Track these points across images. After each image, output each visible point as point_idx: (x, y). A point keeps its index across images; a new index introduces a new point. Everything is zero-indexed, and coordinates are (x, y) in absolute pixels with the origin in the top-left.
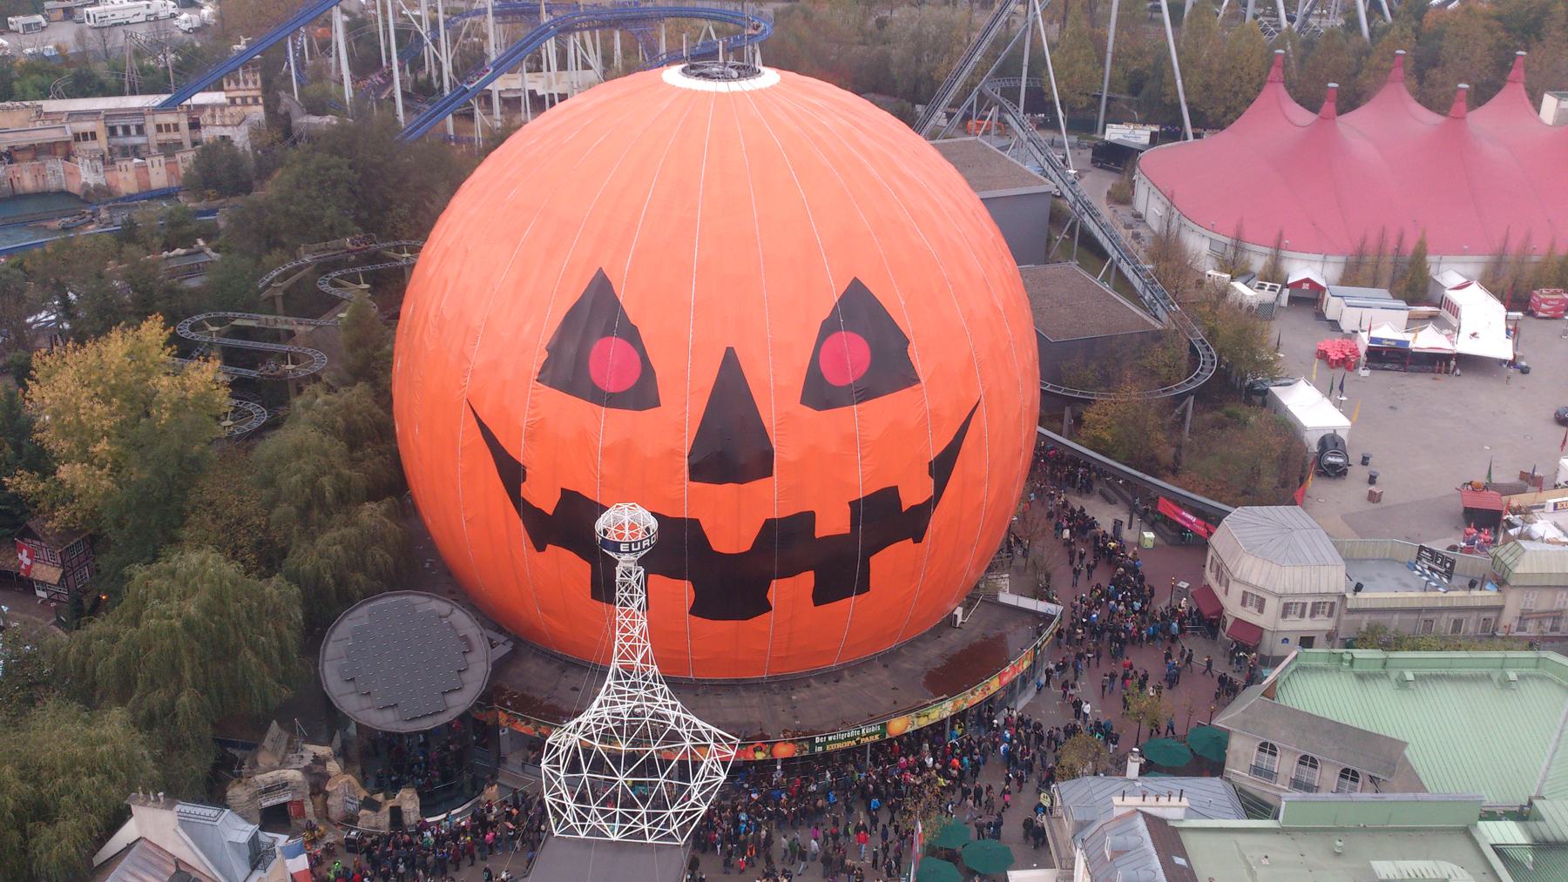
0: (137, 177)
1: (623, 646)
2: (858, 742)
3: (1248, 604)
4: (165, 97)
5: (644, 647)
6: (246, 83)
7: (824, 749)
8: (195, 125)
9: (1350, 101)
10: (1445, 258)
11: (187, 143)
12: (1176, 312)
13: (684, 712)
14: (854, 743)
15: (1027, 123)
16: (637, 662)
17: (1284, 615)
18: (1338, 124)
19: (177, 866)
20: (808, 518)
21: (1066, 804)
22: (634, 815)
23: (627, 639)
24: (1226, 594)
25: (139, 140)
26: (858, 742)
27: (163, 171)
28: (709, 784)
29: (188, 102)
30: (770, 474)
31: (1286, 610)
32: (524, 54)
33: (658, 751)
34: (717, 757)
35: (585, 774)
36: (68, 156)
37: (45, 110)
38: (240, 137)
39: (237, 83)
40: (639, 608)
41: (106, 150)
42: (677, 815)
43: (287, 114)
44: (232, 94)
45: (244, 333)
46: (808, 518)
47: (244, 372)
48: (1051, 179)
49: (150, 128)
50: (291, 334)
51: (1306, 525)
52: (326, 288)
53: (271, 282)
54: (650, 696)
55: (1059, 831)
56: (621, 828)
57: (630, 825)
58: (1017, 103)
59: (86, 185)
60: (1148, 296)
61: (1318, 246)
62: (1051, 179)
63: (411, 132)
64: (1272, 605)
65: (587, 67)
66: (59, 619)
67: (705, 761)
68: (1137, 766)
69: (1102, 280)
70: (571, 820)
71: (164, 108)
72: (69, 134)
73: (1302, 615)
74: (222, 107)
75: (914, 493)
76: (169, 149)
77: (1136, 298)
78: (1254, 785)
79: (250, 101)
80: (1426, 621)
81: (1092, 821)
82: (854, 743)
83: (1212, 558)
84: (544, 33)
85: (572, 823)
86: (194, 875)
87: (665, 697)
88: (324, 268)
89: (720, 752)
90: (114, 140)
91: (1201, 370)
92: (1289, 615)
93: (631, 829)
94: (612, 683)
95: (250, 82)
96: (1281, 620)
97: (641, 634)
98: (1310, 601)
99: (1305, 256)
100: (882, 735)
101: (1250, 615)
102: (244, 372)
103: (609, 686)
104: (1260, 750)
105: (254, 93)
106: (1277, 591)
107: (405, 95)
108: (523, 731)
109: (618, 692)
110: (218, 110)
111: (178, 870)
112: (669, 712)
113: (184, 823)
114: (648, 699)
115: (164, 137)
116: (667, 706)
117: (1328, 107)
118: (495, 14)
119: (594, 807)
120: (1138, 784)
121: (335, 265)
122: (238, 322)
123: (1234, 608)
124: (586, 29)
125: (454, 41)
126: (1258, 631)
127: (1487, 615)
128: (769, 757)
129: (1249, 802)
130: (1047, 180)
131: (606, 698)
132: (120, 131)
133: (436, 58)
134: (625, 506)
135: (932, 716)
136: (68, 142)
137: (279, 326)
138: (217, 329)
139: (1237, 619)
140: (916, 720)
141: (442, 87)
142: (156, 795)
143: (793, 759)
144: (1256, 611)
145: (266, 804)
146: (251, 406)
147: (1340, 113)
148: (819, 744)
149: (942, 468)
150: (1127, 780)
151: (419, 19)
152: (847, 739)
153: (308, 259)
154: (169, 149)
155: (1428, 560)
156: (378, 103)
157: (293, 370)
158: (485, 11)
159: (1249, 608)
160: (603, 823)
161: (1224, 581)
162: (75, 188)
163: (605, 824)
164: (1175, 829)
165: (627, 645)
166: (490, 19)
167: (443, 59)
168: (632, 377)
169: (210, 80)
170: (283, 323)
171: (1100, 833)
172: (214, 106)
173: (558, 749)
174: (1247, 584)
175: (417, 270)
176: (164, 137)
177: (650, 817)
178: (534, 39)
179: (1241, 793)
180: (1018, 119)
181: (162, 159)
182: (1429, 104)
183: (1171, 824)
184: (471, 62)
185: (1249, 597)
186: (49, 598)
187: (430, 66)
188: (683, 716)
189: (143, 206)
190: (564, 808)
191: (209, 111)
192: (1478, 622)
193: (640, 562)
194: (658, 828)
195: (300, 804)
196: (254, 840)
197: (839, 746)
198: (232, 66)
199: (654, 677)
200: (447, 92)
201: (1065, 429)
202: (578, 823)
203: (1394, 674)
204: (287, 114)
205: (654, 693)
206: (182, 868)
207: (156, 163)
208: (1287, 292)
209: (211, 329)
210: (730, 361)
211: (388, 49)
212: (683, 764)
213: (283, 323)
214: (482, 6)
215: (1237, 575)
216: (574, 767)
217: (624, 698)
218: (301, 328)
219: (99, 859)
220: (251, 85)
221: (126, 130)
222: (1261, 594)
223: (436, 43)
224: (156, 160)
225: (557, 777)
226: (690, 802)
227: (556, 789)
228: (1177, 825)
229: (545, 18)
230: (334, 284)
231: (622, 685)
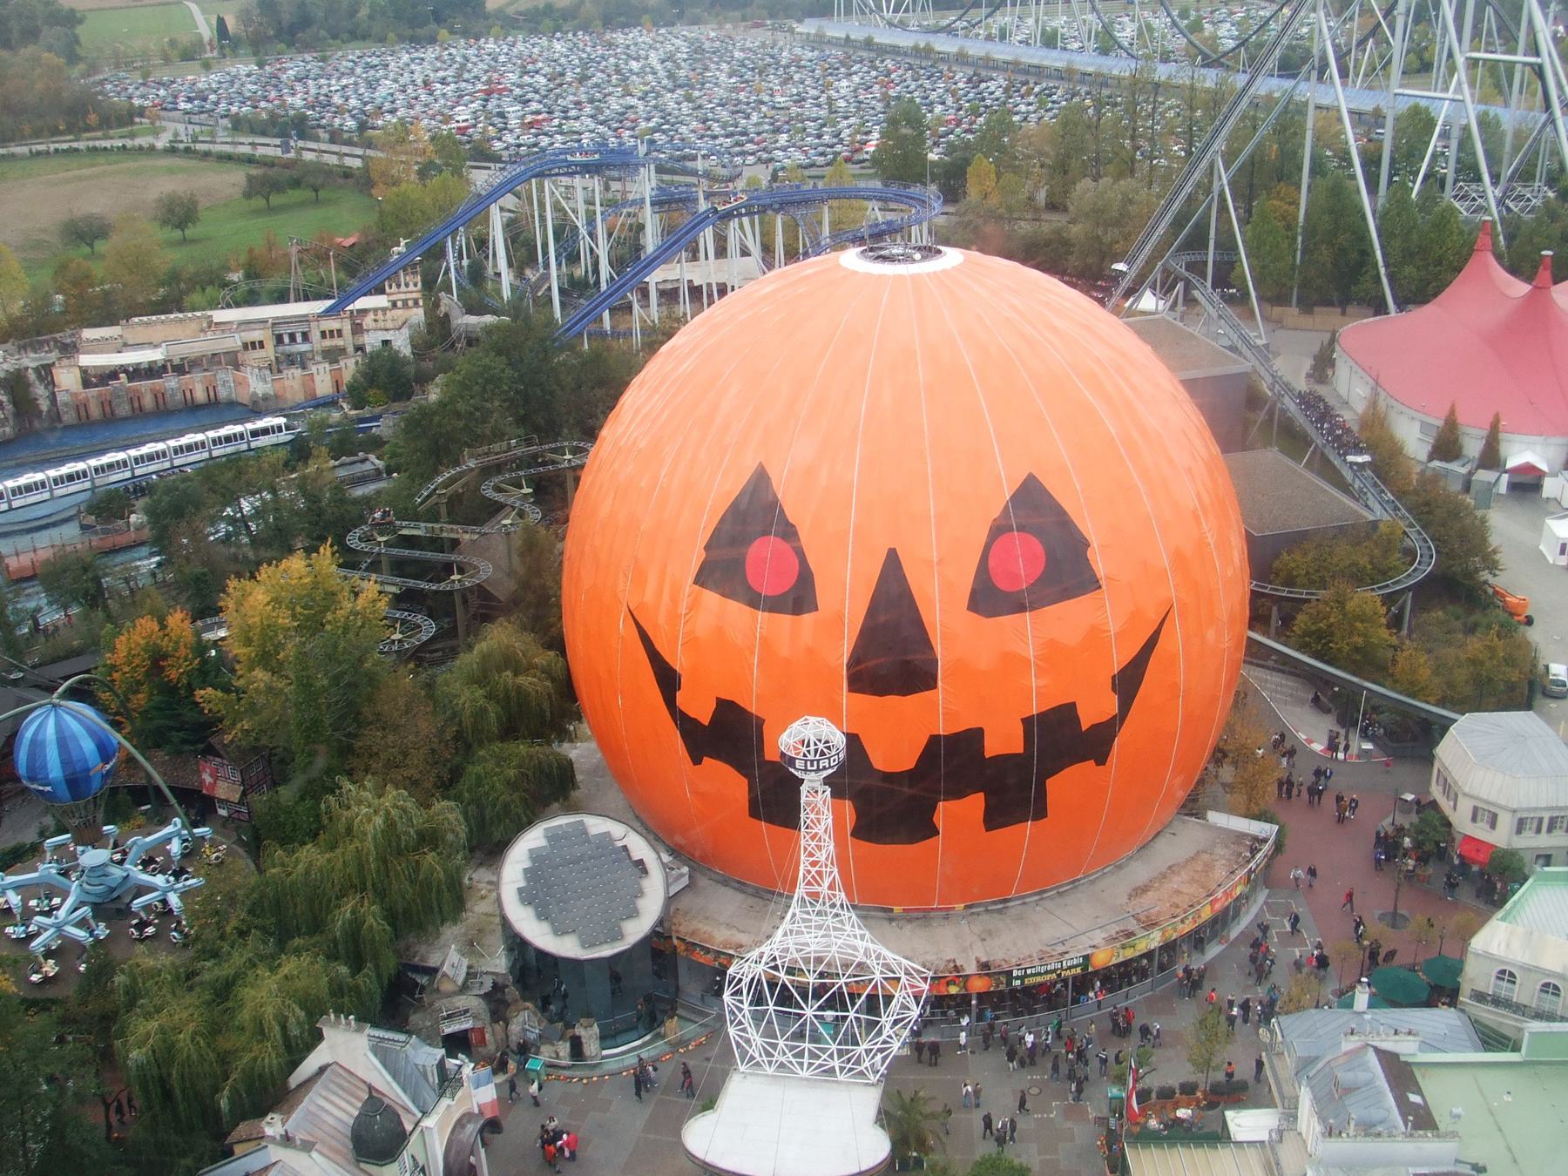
0: (303, 384)
1: (809, 872)
2: (1059, 976)
3: (1479, 818)
4: (329, 303)
5: (831, 873)
6: (407, 285)
7: (1022, 983)
8: (358, 329)
11: (350, 349)
12: (1388, 502)
13: (872, 942)
14: (1054, 976)
15: (1216, 298)
16: (824, 888)
17: (1519, 831)
18: (1555, 296)
19: (370, 1093)
20: (976, 735)
21: (1288, 1040)
22: (823, 1050)
23: (814, 864)
24: (1455, 808)
25: (305, 347)
26: (1059, 976)
27: (328, 378)
28: (903, 1019)
29: (350, 307)
30: (935, 687)
31: (1520, 827)
32: (680, 242)
33: (846, 984)
34: (909, 991)
35: (771, 1007)
36: (237, 366)
37: (216, 320)
38: (402, 343)
39: (399, 286)
40: (826, 831)
41: (273, 358)
42: (868, 1051)
43: (446, 315)
44: (393, 298)
45: (410, 542)
46: (976, 735)
47: (411, 583)
48: (1245, 358)
49: (315, 336)
50: (455, 543)
52: (490, 493)
53: (435, 490)
54: (839, 926)
55: (1281, 1069)
56: (810, 1064)
57: (820, 1061)
59: (255, 394)
60: (1357, 484)
61: (1538, 428)
62: (1245, 358)
63: (569, 329)
64: (1506, 822)
65: (745, 253)
66: (240, 839)
67: (897, 995)
68: (1366, 997)
69: (1306, 466)
70: (756, 1055)
71: (328, 313)
72: (240, 344)
73: (1538, 831)
74: (384, 310)
75: (1096, 707)
76: (332, 355)
77: (1345, 487)
78: (1489, 1015)
79: (410, 303)
81: (1317, 1058)
82: (1054, 976)
84: (700, 222)
85: (759, 1059)
86: (386, 1101)
87: (853, 926)
88: (487, 472)
89: (912, 986)
90: (280, 348)
91: (1420, 563)
93: (821, 1066)
94: (797, 911)
95: (411, 284)
97: (827, 859)
98: (1546, 816)
99: (1524, 438)
100: (1085, 968)
101: (1480, 832)
102: (411, 583)
103: (794, 915)
104: (1498, 978)
105: (415, 295)
106: (1510, 805)
107: (561, 290)
108: (701, 961)
109: (804, 920)
110: (380, 312)
111: (371, 1096)
112: (858, 942)
113: (378, 1049)
114: (835, 929)
115: (328, 343)
116: (855, 936)
117: (1545, 275)
118: (653, 204)
119: (781, 1043)
120: (1366, 1016)
121: (498, 468)
122: (405, 532)
123: (1461, 821)
124: (746, 215)
125: (610, 235)
128: (963, 992)
129: (1483, 1034)
130: (1242, 360)
131: (791, 927)
132: (286, 339)
133: (591, 250)
134: (812, 719)
135: (1138, 948)
136: (236, 353)
137: (444, 535)
138: (385, 539)
140: (1121, 951)
141: (597, 282)
142: (347, 1018)
143: (988, 993)
144: (1487, 827)
145: (448, 1031)
146: (419, 619)
147: (1555, 283)
148: (1017, 978)
149: (1128, 682)
150: (1356, 1013)
151: (575, 211)
152: (1047, 972)
153: (472, 464)
154: (332, 355)
156: (534, 301)
157: (459, 581)
158: (643, 200)
159: (1479, 824)
160: (792, 1059)
162: (244, 398)
163: (794, 1061)
164: (1408, 1064)
165: (813, 870)
168: (790, 580)
169: (372, 285)
170: (448, 531)
171: (1327, 1069)
172: (375, 310)
173: (740, 980)
174: (1477, 798)
175: (587, 479)
176: (328, 343)
177: (841, 1053)
178: (693, 228)
179: (1476, 1023)
180: (1204, 292)
181: (327, 365)
183: (1402, 1059)
184: (629, 256)
186: (230, 816)
188: (871, 946)
189: (310, 413)
190: (748, 1041)
191: (371, 316)
193: (827, 781)
194: (849, 1066)
195: (481, 1031)
196: (441, 1066)
197: (1039, 979)
198: (393, 270)
199: (842, 906)
200: (604, 287)
201: (1273, 630)
202: (765, 1059)
204: (446, 315)
205: (842, 922)
206: (375, 1094)
207: (322, 370)
208: (1505, 477)
209: (380, 539)
210: (893, 560)
211: (545, 245)
212: (872, 998)
213: (448, 531)
214: (638, 196)
215: (1466, 790)
216: (759, 1000)
217: (810, 927)
218: (467, 537)
219: (295, 1079)
220: (411, 288)
221: (292, 337)
222: (1493, 809)
223: (592, 235)
224: (321, 367)
225: (741, 1010)
226: (881, 1039)
227: (740, 1023)
228: (1410, 1060)
229: (703, 206)
230: (499, 490)
231: (808, 913)
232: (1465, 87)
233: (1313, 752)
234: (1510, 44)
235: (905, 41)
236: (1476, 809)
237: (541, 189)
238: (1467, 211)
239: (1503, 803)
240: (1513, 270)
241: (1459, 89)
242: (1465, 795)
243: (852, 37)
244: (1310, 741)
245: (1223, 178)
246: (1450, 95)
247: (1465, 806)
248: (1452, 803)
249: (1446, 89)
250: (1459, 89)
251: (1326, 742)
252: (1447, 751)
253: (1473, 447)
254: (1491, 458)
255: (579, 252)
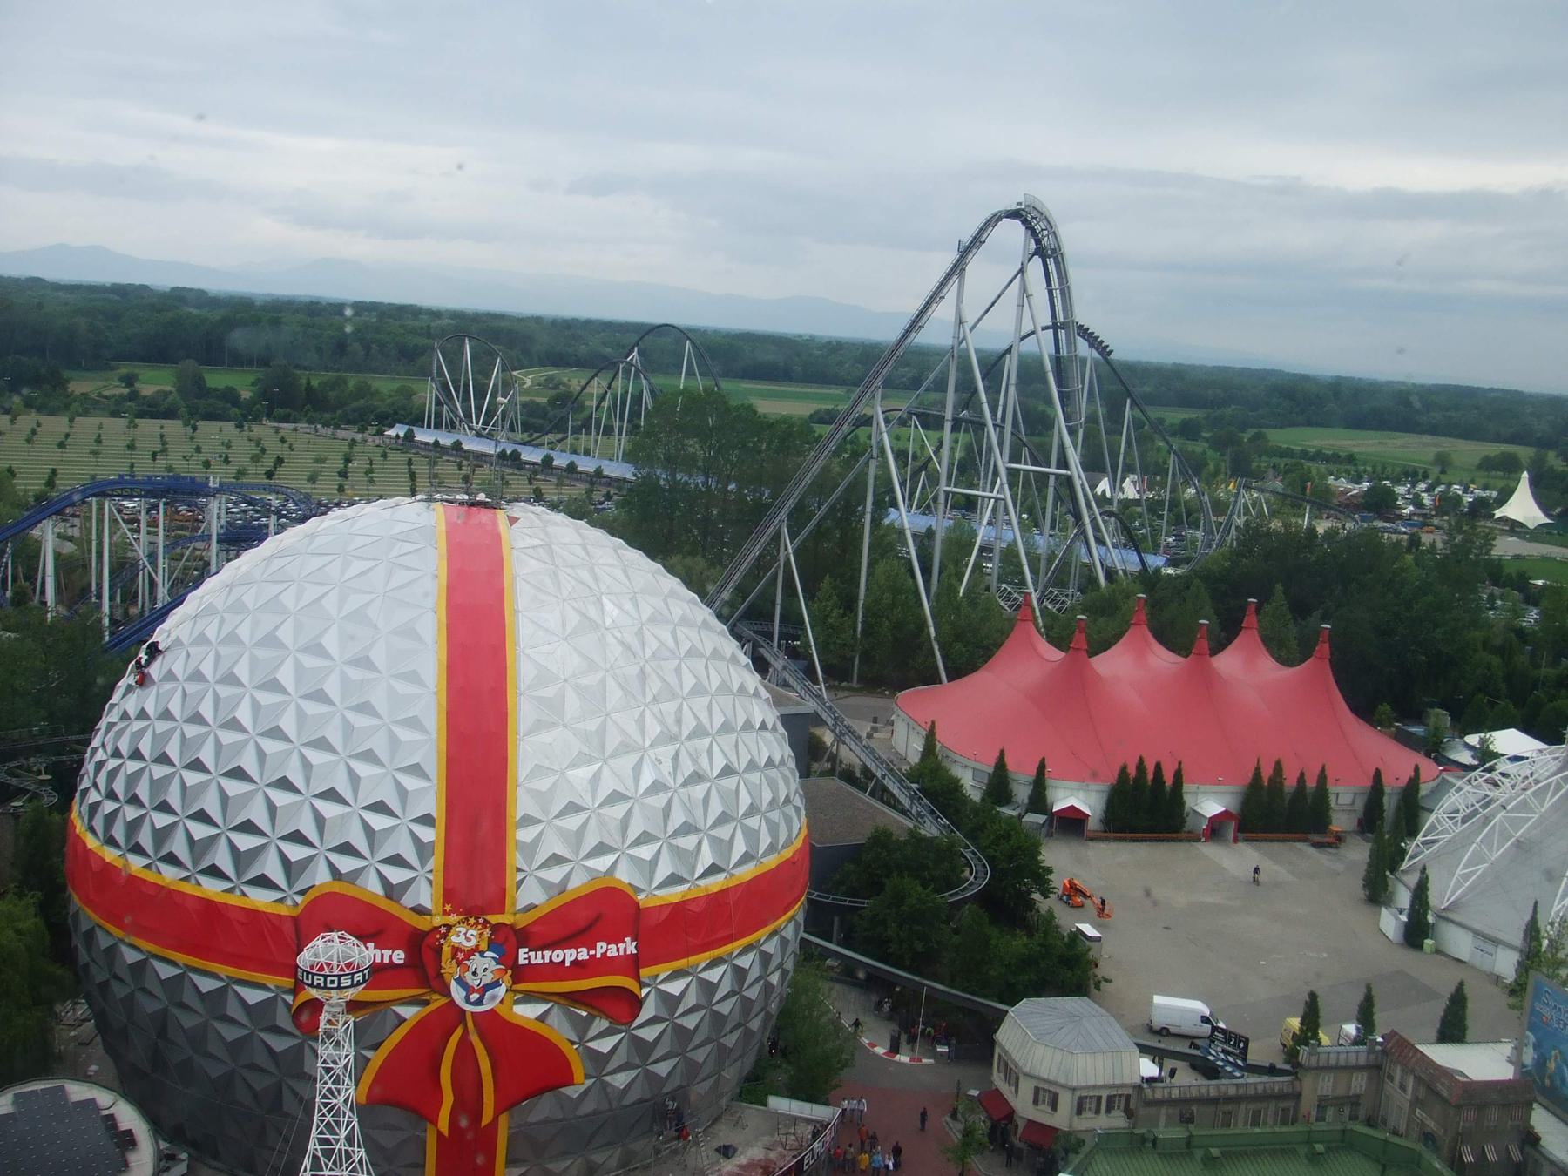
9: (1100, 646)
10: (1202, 788)
12: (944, 826)
24: (1017, 1092)
51: (1094, 1013)
57: (331, 1137)
58: (771, 639)
61: (1082, 775)
64: (1066, 1102)
69: (870, 794)
73: (1097, 1112)
80: (1224, 1113)
83: (1000, 1056)
92: (1084, 1112)
96: (1076, 1117)
98: (1105, 1094)
99: (1067, 784)
101: (1042, 1116)
123: (1023, 1104)
126: (1051, 1131)
127: (1282, 1105)
139: (1029, 1121)
155: (1221, 1042)
158: (209, 537)
159: (1042, 1107)
161: (1013, 1081)
166: (214, 546)
167: (159, 579)
174: (1038, 1078)
182: (1173, 648)
185: (1041, 1093)
187: (143, 598)
192: (1276, 1113)
203: (1199, 1153)
215: (1027, 1069)
232: (1006, 487)
233: (876, 1055)
234: (1041, 457)
235: (487, 448)
236: (1037, 1090)
237: (101, 509)
238: (1010, 607)
239: (1062, 1081)
240: (1051, 641)
241: (1001, 490)
242: (1026, 1075)
243: (441, 443)
244: (873, 1046)
245: (788, 548)
246: (994, 494)
247: (1026, 1088)
248: (1013, 1089)
249: (992, 491)
250: (1001, 490)
251: (888, 1046)
252: (1007, 1036)
253: (1022, 793)
254: (1038, 801)
255: (136, 593)
